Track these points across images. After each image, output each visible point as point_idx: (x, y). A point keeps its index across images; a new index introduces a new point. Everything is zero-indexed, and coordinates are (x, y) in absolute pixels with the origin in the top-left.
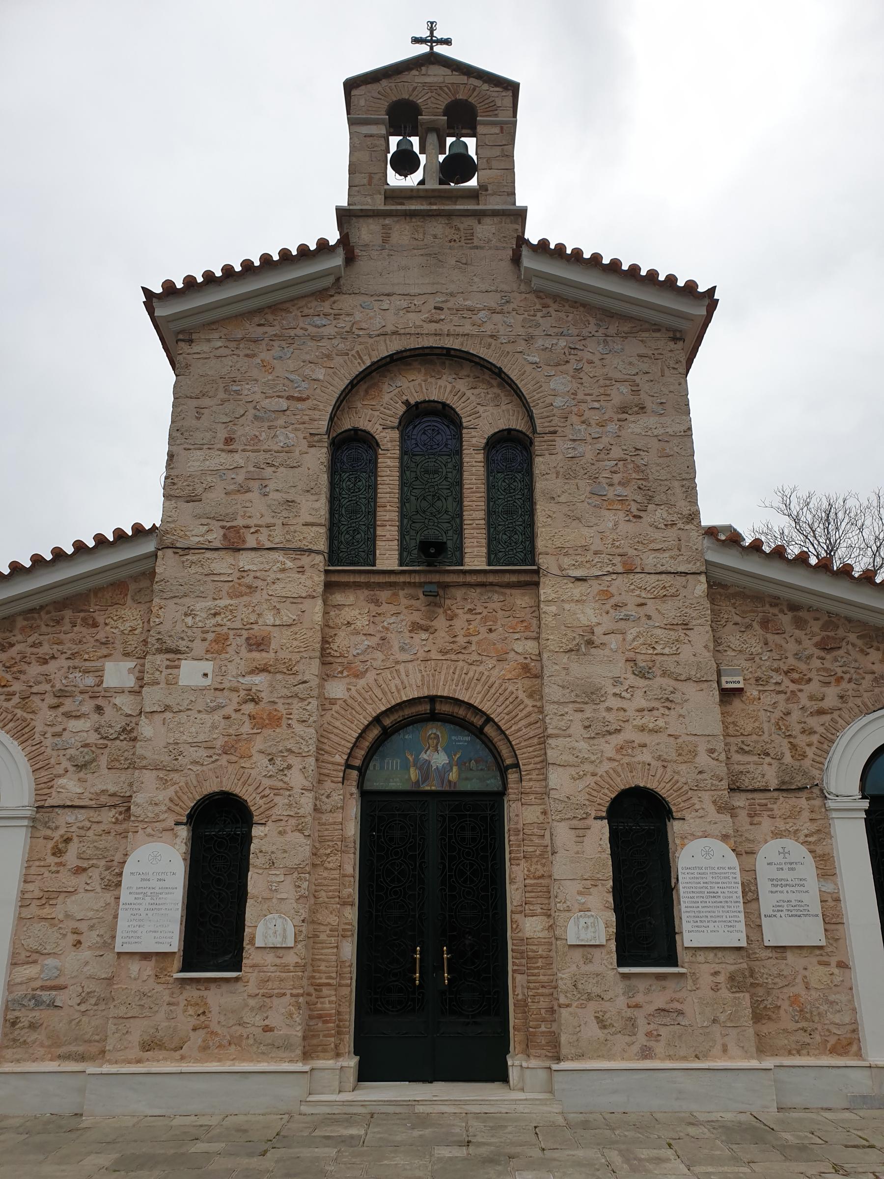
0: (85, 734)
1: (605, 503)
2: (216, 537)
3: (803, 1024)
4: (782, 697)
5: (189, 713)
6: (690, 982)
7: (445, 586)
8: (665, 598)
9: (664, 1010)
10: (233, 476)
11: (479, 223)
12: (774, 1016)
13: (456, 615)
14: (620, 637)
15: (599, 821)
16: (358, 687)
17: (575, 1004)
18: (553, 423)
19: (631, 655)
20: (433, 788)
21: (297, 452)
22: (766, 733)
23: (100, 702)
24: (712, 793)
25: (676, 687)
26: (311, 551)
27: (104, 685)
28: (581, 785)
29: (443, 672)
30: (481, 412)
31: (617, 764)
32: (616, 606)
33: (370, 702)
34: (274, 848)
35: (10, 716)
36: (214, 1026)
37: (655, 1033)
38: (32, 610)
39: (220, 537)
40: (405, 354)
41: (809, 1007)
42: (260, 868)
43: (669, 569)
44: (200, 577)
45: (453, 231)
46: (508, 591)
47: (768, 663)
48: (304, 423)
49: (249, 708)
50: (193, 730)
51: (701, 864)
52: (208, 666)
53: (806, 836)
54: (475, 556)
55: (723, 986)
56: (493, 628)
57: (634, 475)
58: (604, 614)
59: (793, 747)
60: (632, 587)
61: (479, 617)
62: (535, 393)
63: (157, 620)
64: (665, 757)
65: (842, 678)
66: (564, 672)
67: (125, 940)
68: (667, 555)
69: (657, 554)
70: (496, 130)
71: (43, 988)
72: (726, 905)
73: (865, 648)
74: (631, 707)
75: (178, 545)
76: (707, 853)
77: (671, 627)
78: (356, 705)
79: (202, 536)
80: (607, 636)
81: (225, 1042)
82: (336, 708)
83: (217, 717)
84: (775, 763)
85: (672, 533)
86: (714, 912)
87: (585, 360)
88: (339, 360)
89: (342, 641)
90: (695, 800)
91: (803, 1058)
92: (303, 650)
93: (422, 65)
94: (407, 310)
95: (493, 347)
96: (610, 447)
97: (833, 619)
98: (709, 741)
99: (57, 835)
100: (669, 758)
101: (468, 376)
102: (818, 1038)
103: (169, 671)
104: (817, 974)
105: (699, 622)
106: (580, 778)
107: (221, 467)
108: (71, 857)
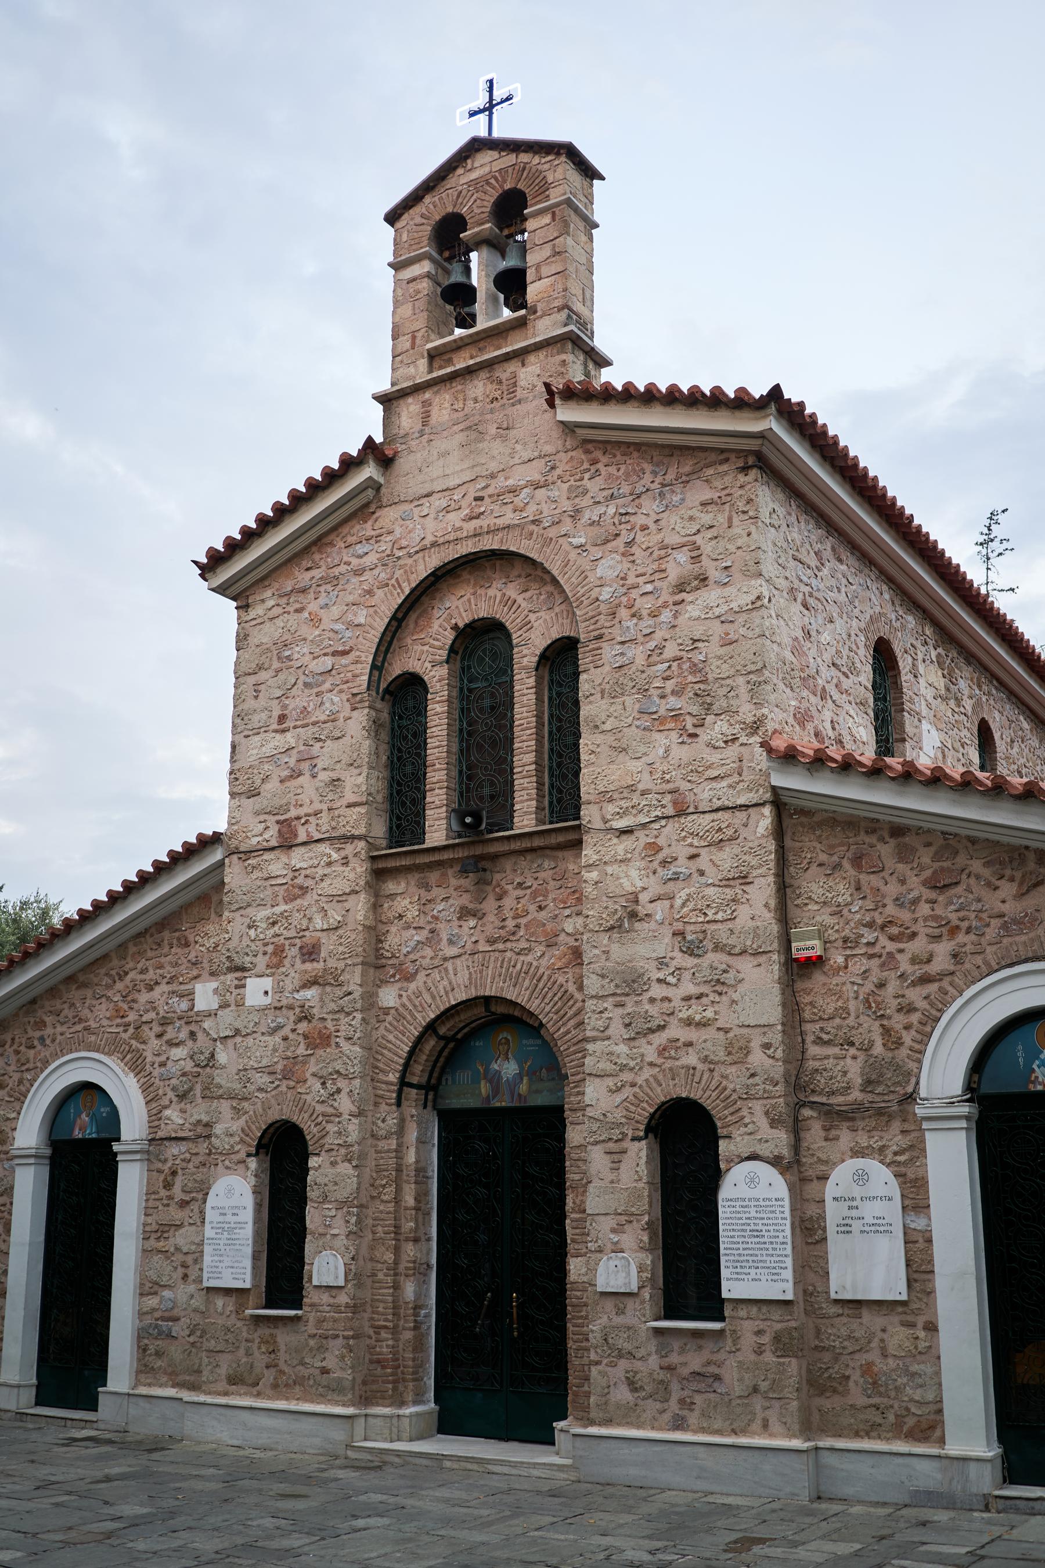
0: (182, 1062)
1: (657, 723)
2: (272, 836)
3: (876, 1400)
4: (876, 962)
5: (254, 1035)
6: (729, 1341)
7: (495, 857)
8: (722, 844)
9: (699, 1374)
10: (286, 760)
11: (523, 365)
12: (841, 1389)
13: (505, 892)
14: (667, 903)
15: (636, 1144)
16: (410, 992)
17: (605, 1361)
18: (598, 625)
19: (679, 926)
20: (504, 1104)
21: (342, 720)
22: (853, 1014)
23: (193, 1027)
24: (765, 1102)
25: (730, 963)
26: (353, 838)
27: (196, 1009)
28: (618, 1098)
29: (491, 966)
30: (533, 620)
31: (658, 1070)
32: (664, 863)
33: (420, 1009)
34: (326, 1180)
35: (127, 1048)
36: (283, 1366)
37: (688, 1400)
38: (140, 935)
39: (276, 834)
40: (448, 567)
41: (883, 1379)
42: (316, 1202)
43: (727, 803)
44: (259, 883)
45: (495, 386)
46: (560, 854)
47: (858, 916)
48: (347, 682)
49: (303, 1027)
50: (258, 1054)
51: (750, 1195)
52: (267, 983)
53: (896, 1154)
54: (526, 816)
55: (768, 1348)
56: (544, 904)
57: (690, 678)
58: (651, 874)
59: (886, 1031)
60: (684, 834)
61: (528, 891)
62: (579, 588)
63: (226, 936)
64: (712, 1057)
65: (957, 927)
66: (604, 957)
67: (211, 1275)
68: (724, 783)
69: (714, 784)
70: (547, 219)
71: (163, 1319)
72: (770, 1246)
73: (993, 880)
74: (676, 994)
75: (242, 849)
76: (752, 1181)
77: (727, 883)
78: (406, 1014)
79: (261, 835)
80: (653, 905)
81: (291, 1382)
82: (389, 1018)
83: (277, 1038)
84: (862, 1057)
85: (733, 751)
86: (757, 1256)
87: (638, 527)
88: (380, 593)
89: (397, 939)
90: (745, 1112)
91: (872, 1441)
92: (347, 956)
93: (467, 158)
94: (447, 510)
95: (535, 536)
96: (664, 643)
97: (951, 842)
98: (764, 1033)
99: (166, 1167)
100: (716, 1059)
101: (519, 576)
102: (891, 1418)
103: (238, 991)
104: (898, 1337)
105: (760, 871)
106: (619, 1090)
107: (276, 752)
108: (177, 1191)
